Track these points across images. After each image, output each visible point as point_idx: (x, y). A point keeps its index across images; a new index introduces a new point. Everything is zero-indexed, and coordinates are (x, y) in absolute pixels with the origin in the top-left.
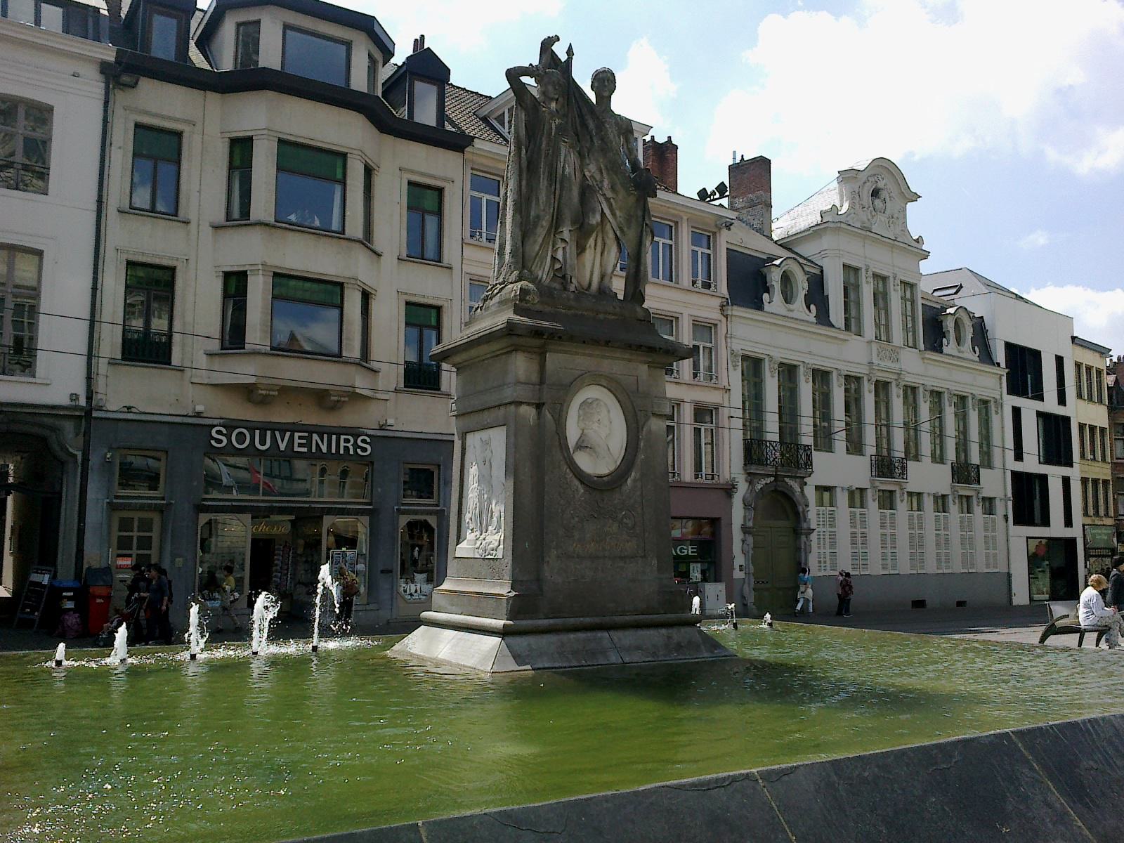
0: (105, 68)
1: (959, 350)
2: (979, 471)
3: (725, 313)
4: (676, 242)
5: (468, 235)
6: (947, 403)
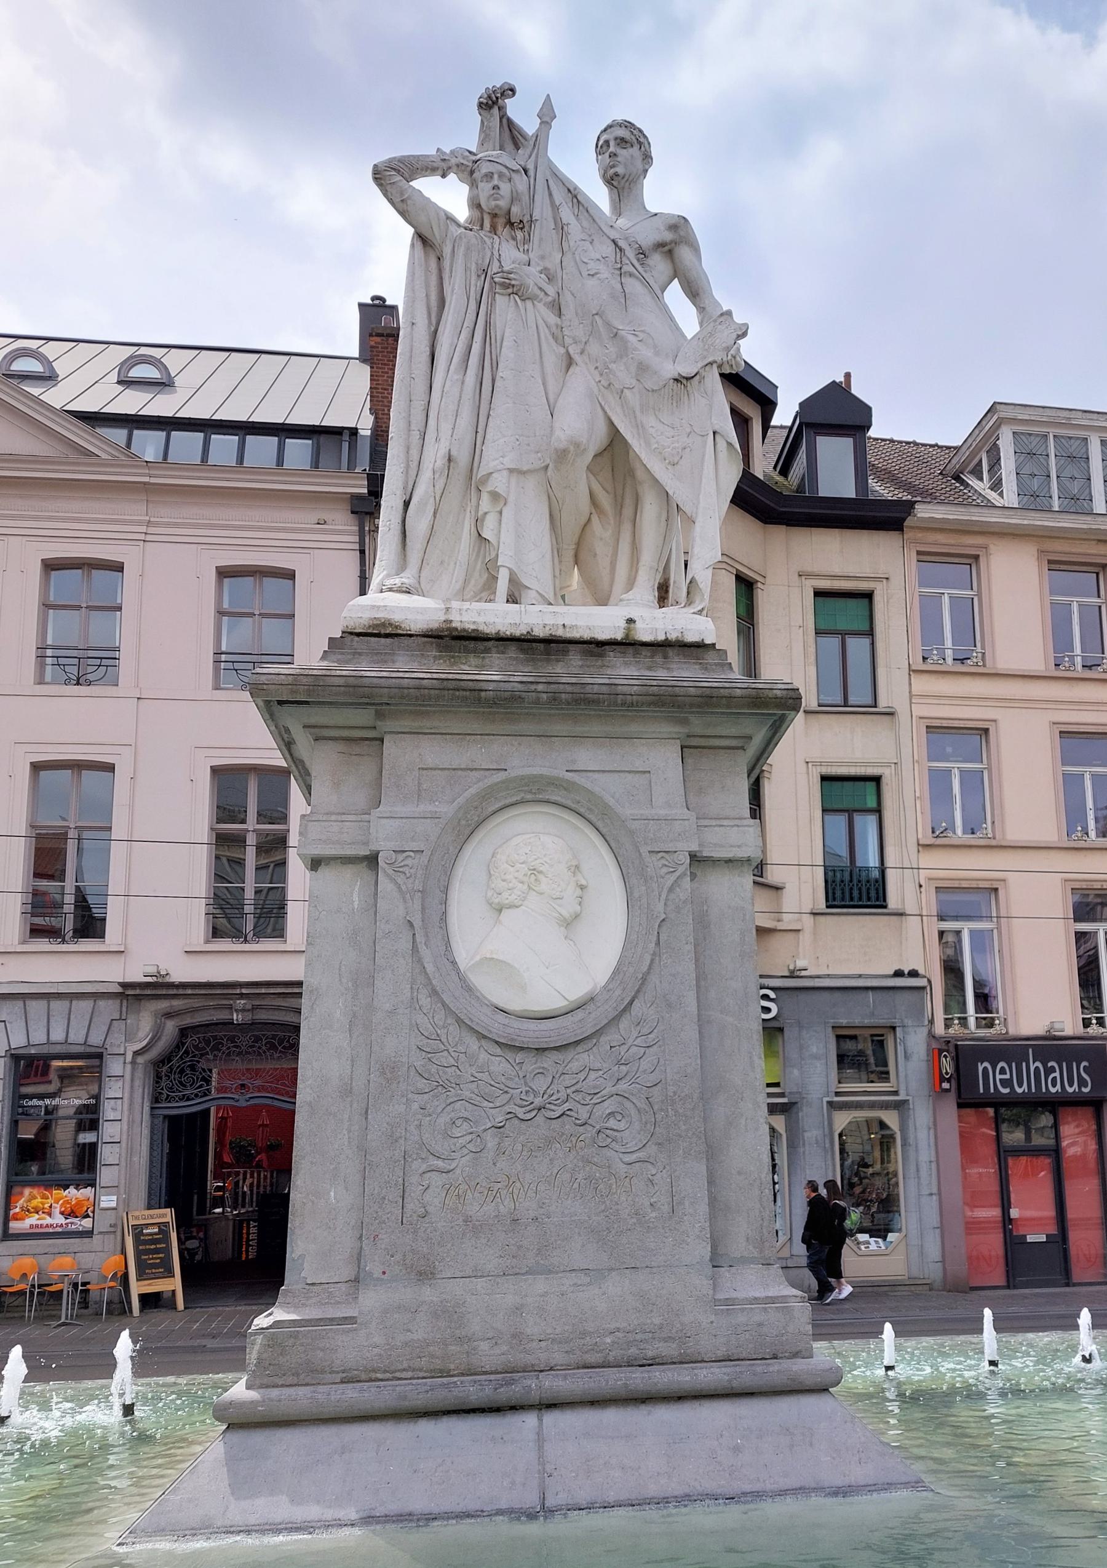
4: (979, 595)
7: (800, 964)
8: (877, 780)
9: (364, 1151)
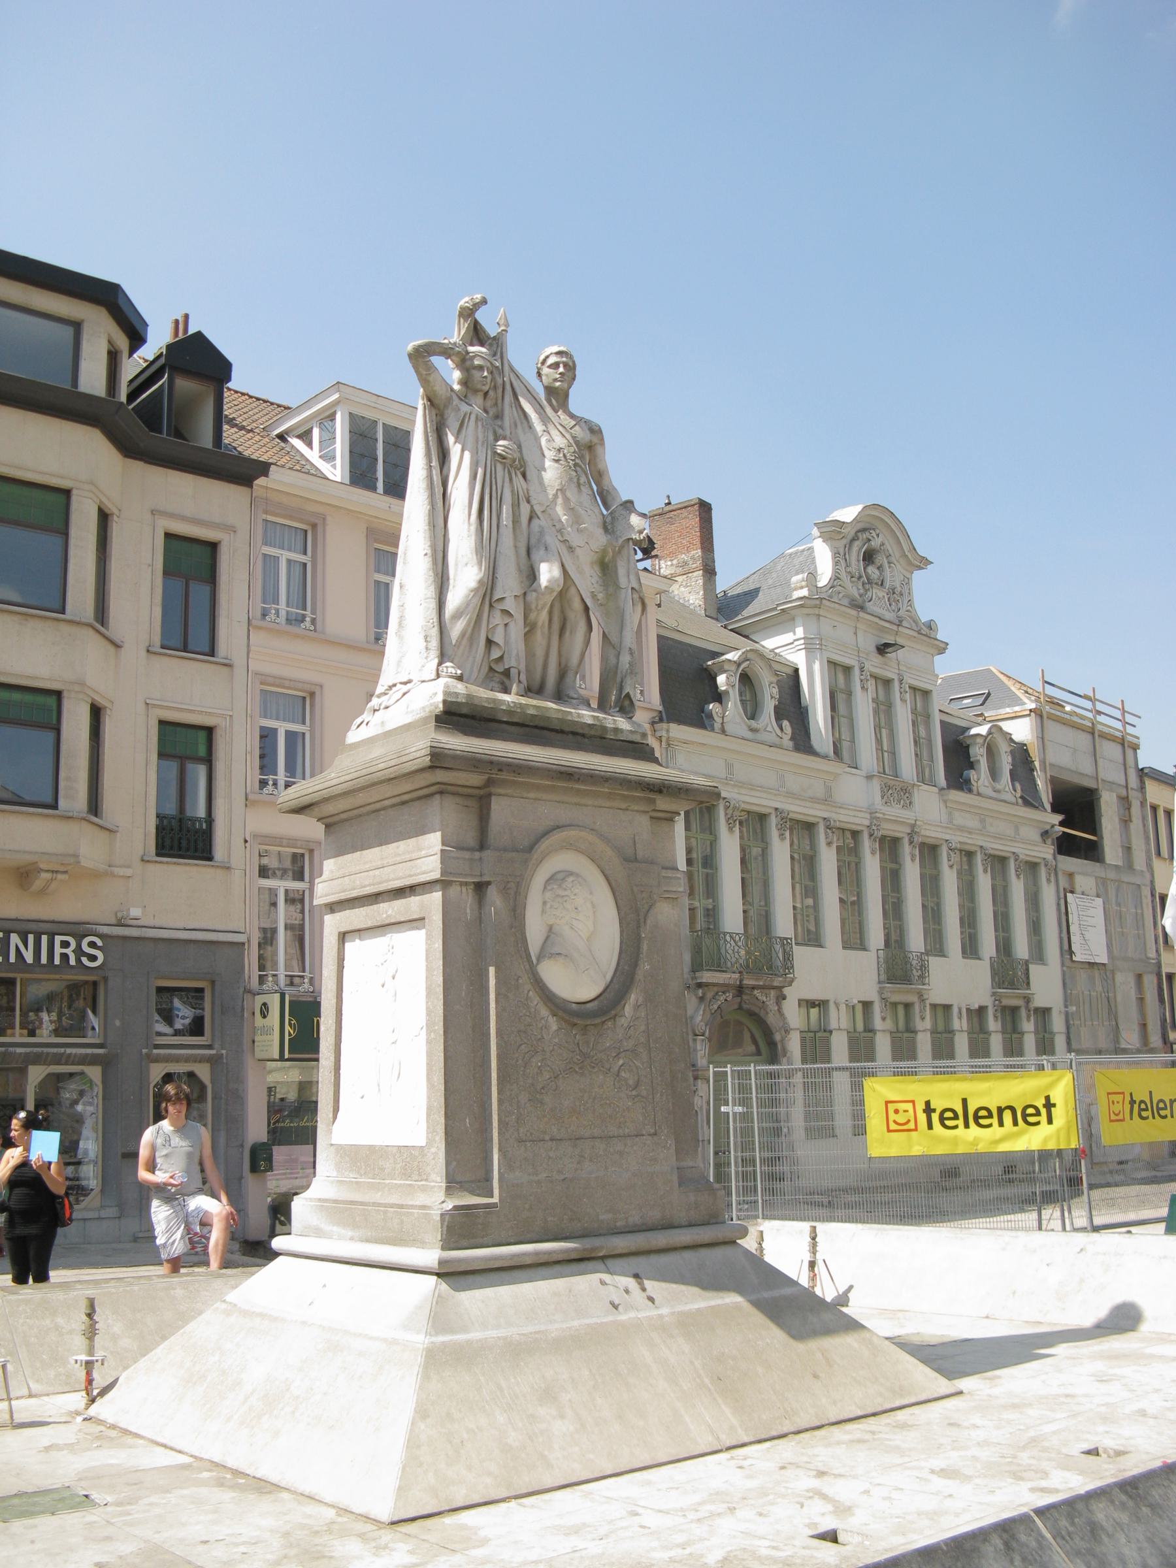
1: (992, 786)
2: (1027, 969)
3: (658, 734)
5: (259, 614)
6: (908, 858)
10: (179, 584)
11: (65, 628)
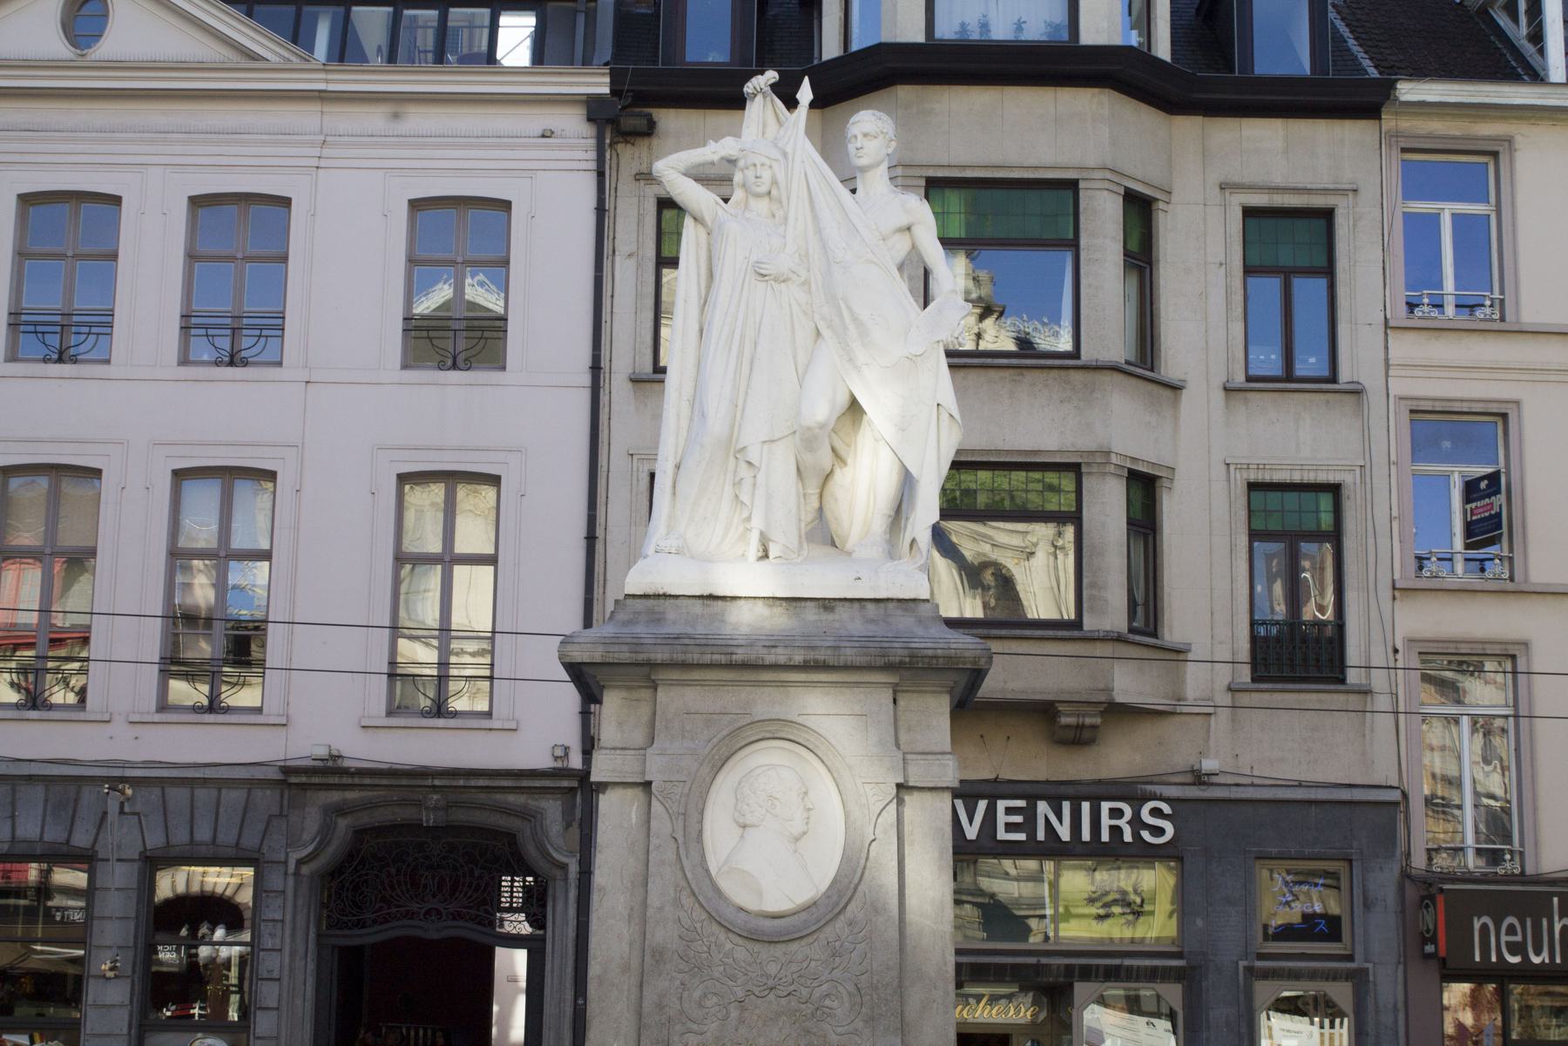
0: (595, 110)
7: (1209, 765)
8: (1335, 489)
9: (640, 1015)
10: (1271, 286)
11: (1077, 376)
